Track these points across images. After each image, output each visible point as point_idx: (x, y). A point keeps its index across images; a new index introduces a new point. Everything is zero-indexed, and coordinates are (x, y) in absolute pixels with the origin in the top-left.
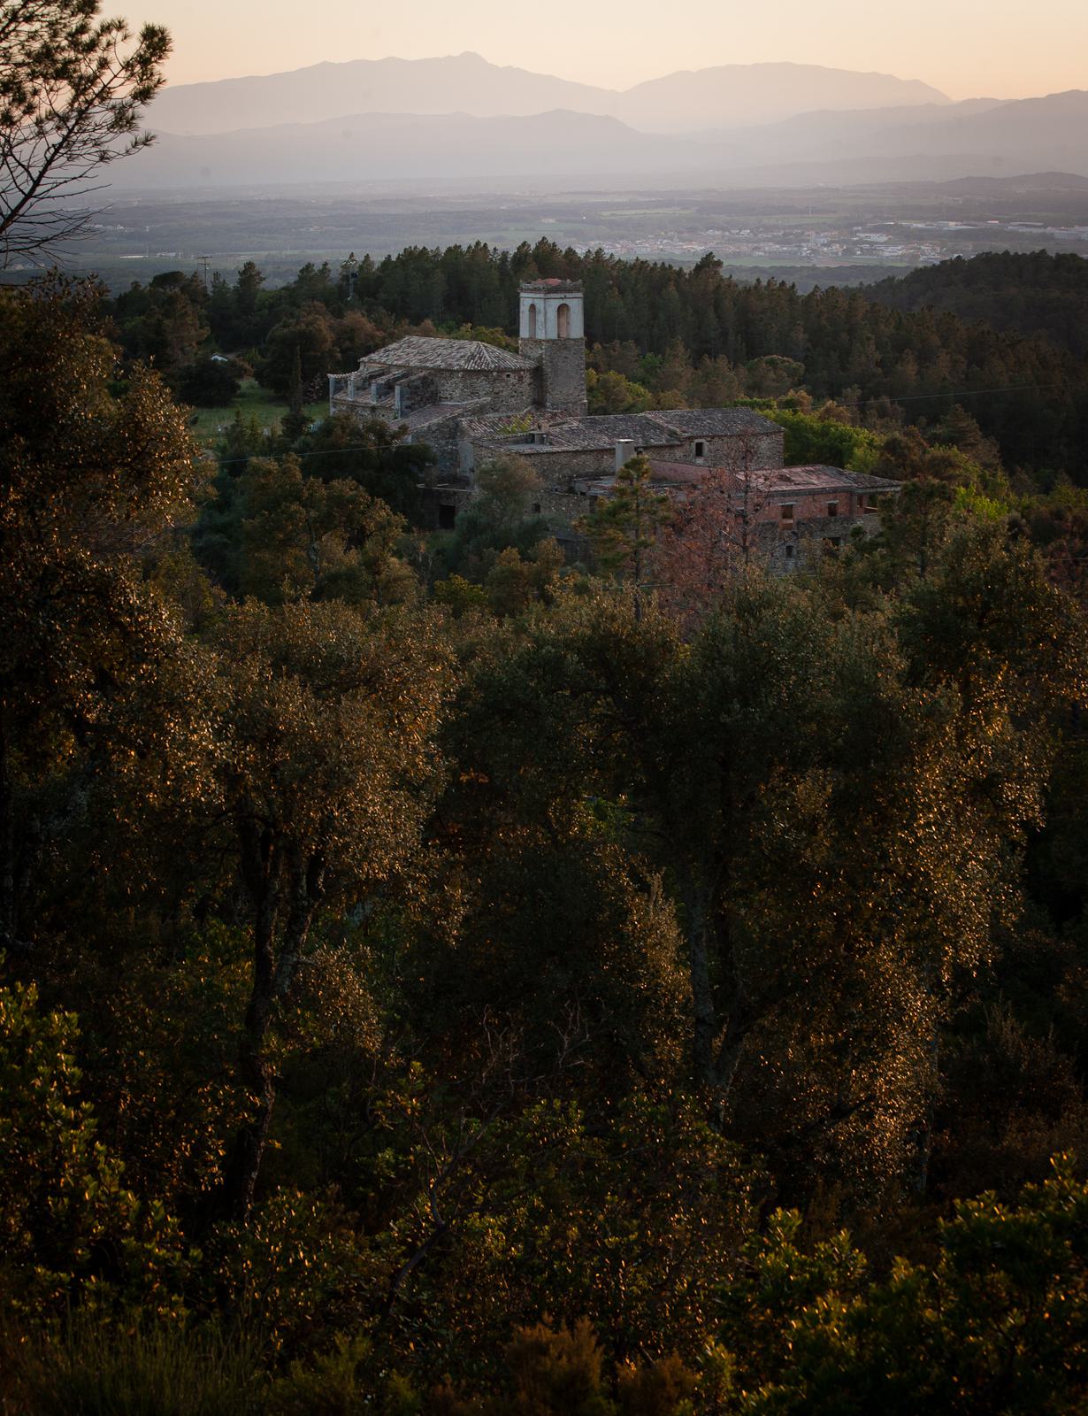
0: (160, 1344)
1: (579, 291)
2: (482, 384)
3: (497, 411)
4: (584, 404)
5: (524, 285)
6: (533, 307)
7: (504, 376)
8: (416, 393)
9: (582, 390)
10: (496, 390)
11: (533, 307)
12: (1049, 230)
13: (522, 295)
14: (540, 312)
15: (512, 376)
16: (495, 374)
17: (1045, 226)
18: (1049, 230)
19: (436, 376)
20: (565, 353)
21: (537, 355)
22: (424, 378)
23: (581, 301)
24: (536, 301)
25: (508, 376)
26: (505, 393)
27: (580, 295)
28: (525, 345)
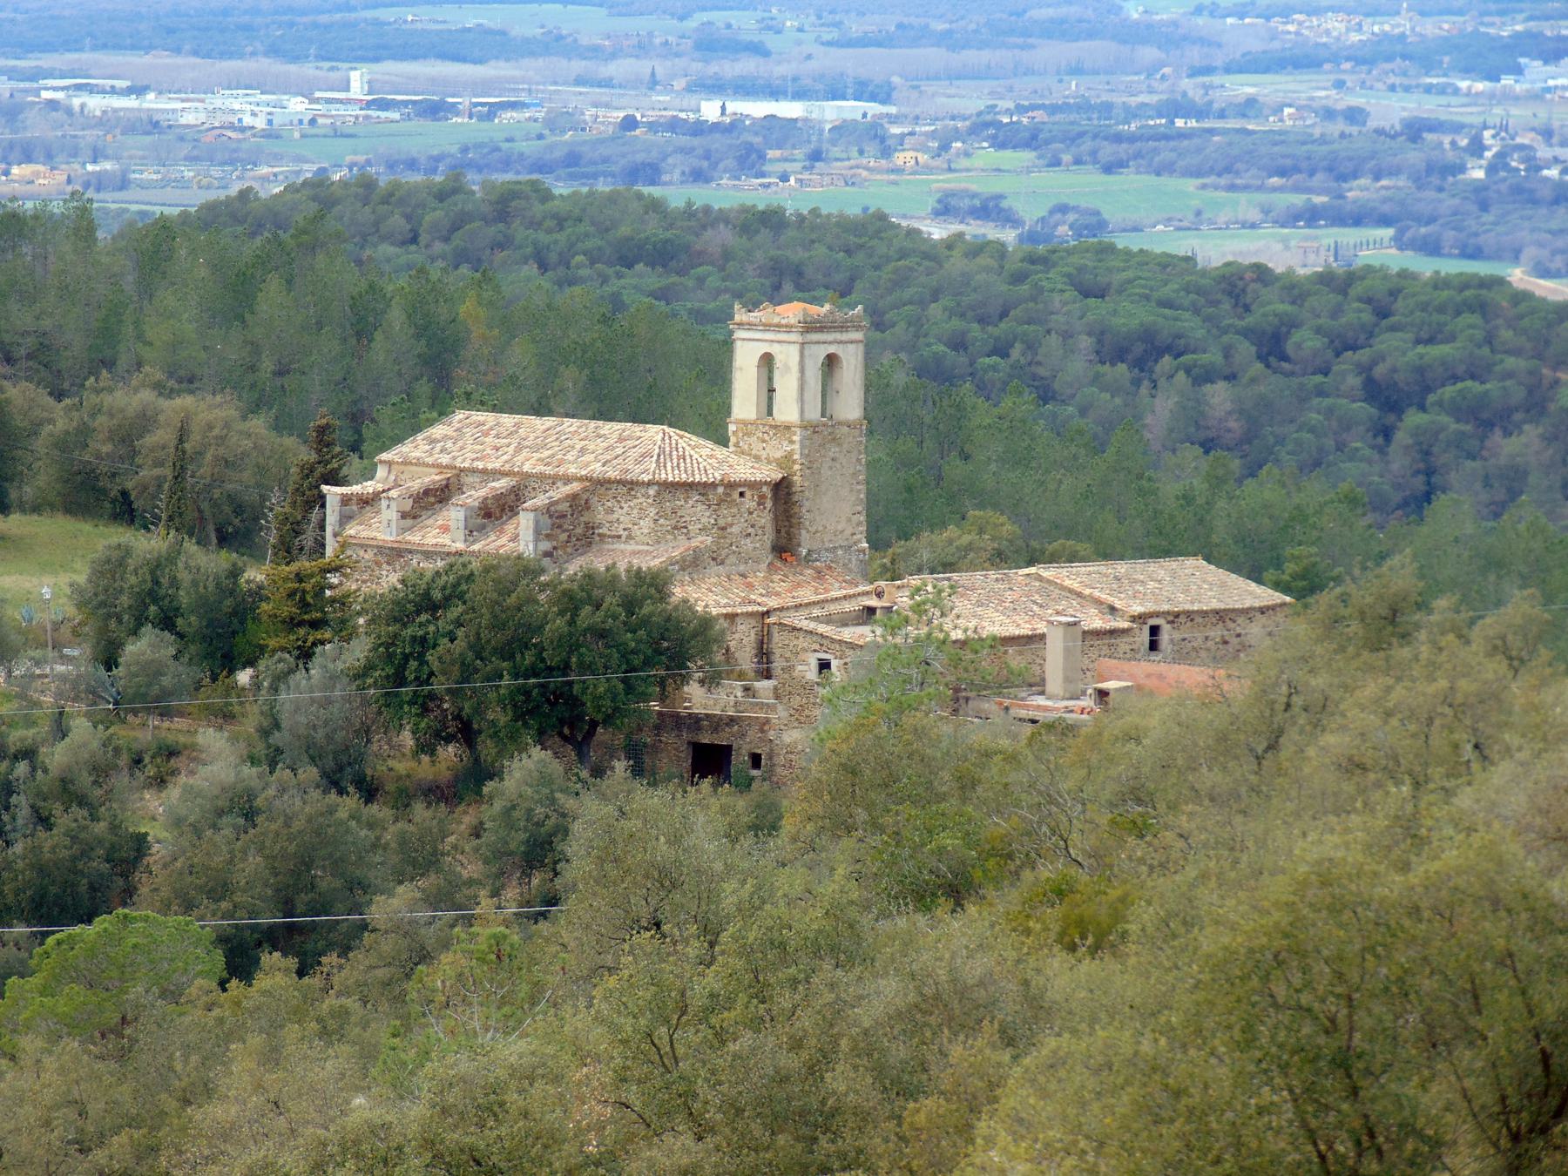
0: (1403, 846)
1: (858, 328)
2: (696, 512)
3: (722, 563)
4: (863, 551)
5: (740, 315)
6: (767, 361)
7: (736, 495)
8: (560, 527)
9: (859, 524)
10: (721, 522)
11: (767, 361)
12: (151, 101)
13: (739, 334)
14: (787, 368)
15: (748, 494)
16: (720, 490)
17: (138, 90)
18: (151, 101)
19: (593, 492)
20: (834, 450)
21: (779, 454)
22: (574, 497)
23: (861, 347)
24: (775, 349)
25: (742, 494)
26: (735, 529)
27: (859, 336)
28: (748, 434)
